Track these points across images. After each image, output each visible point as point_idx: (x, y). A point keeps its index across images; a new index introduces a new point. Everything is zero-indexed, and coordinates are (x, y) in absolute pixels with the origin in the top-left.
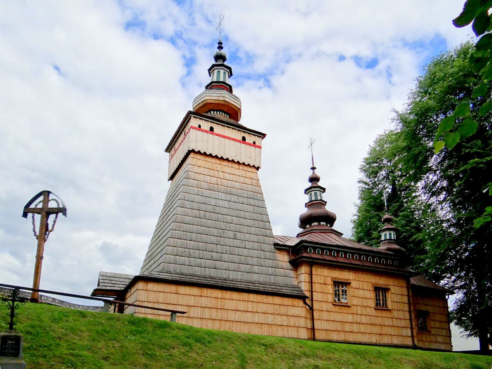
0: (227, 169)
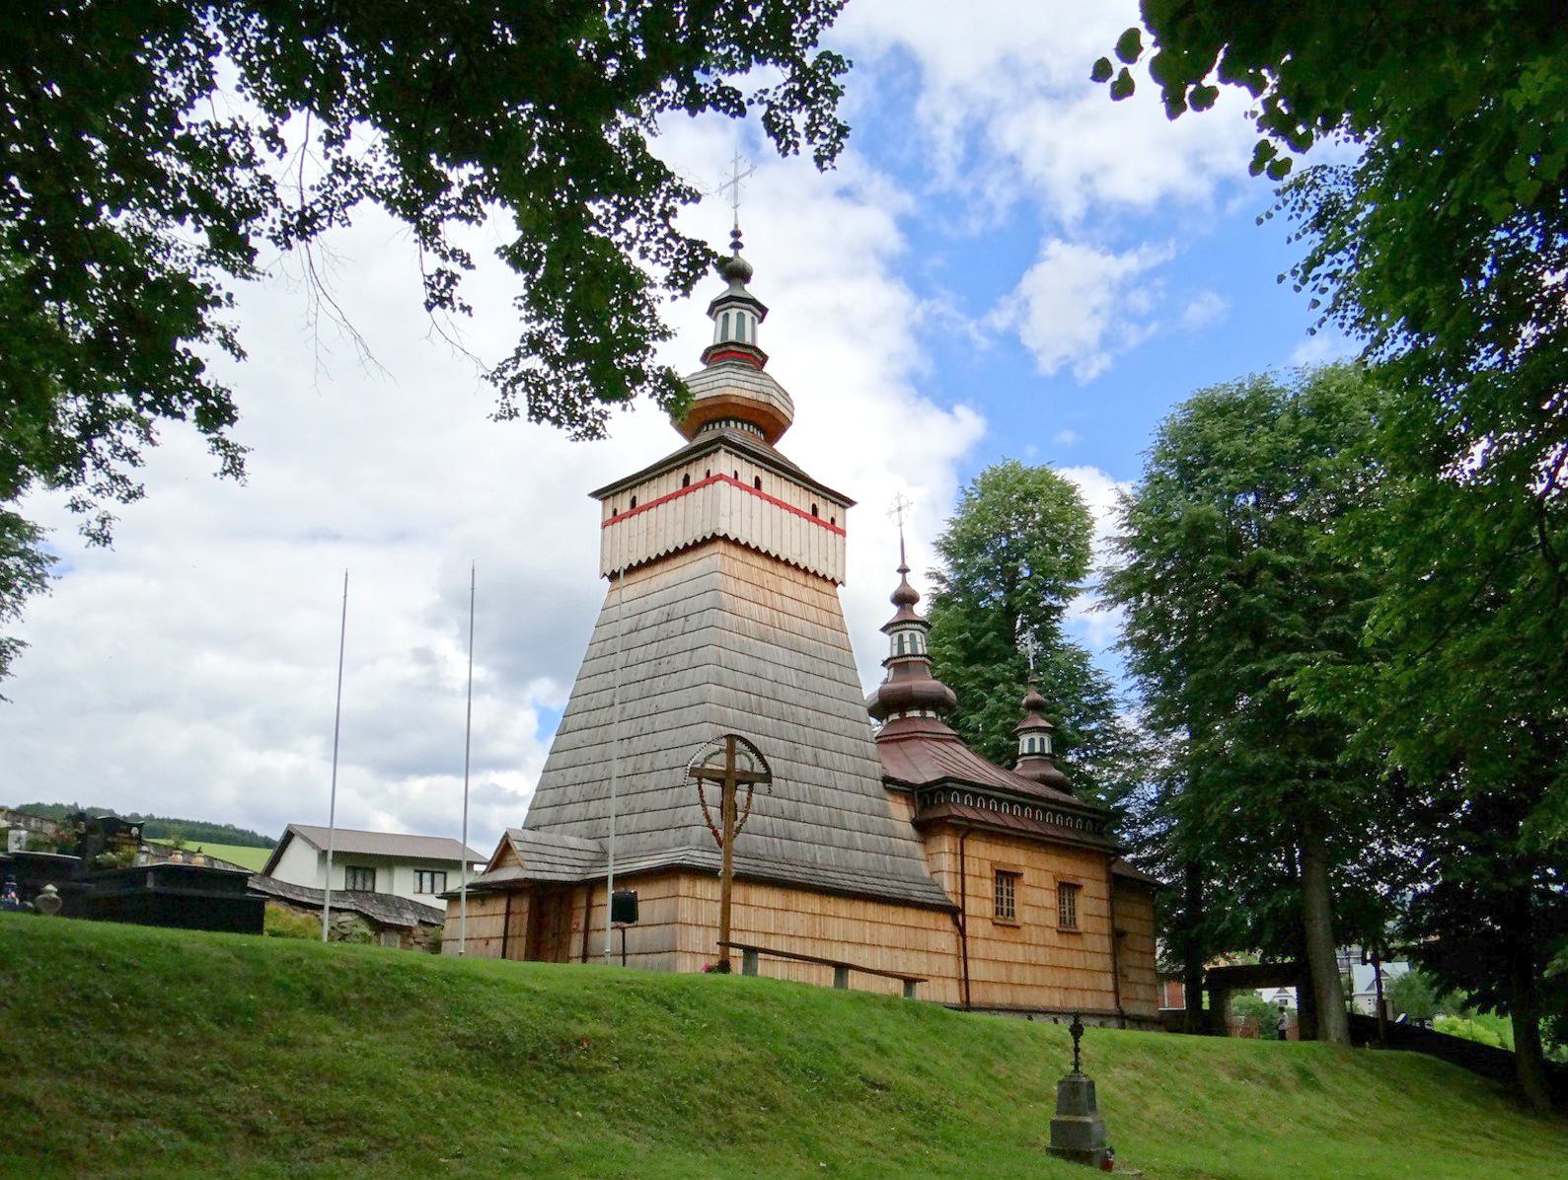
0: (788, 588)
